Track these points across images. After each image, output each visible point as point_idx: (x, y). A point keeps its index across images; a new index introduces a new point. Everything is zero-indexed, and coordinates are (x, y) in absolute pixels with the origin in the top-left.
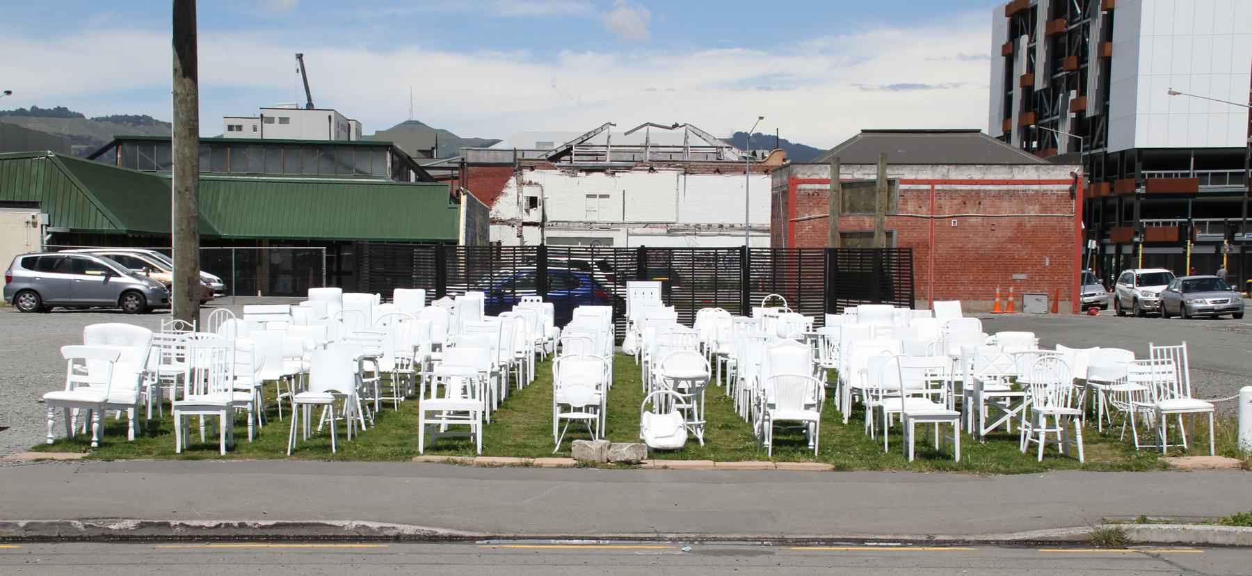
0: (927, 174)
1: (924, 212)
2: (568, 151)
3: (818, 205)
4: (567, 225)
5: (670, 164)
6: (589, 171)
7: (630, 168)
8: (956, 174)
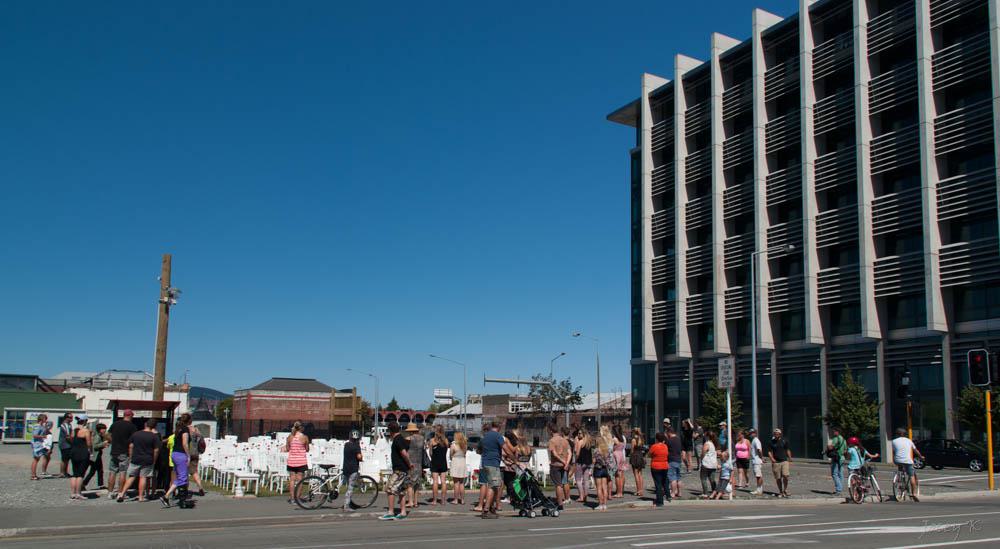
0: (300, 394)
1: (299, 409)
2: (91, 381)
3: (259, 405)
4: (90, 411)
5: (139, 388)
6: (101, 389)
7: (119, 389)
8: (310, 395)
